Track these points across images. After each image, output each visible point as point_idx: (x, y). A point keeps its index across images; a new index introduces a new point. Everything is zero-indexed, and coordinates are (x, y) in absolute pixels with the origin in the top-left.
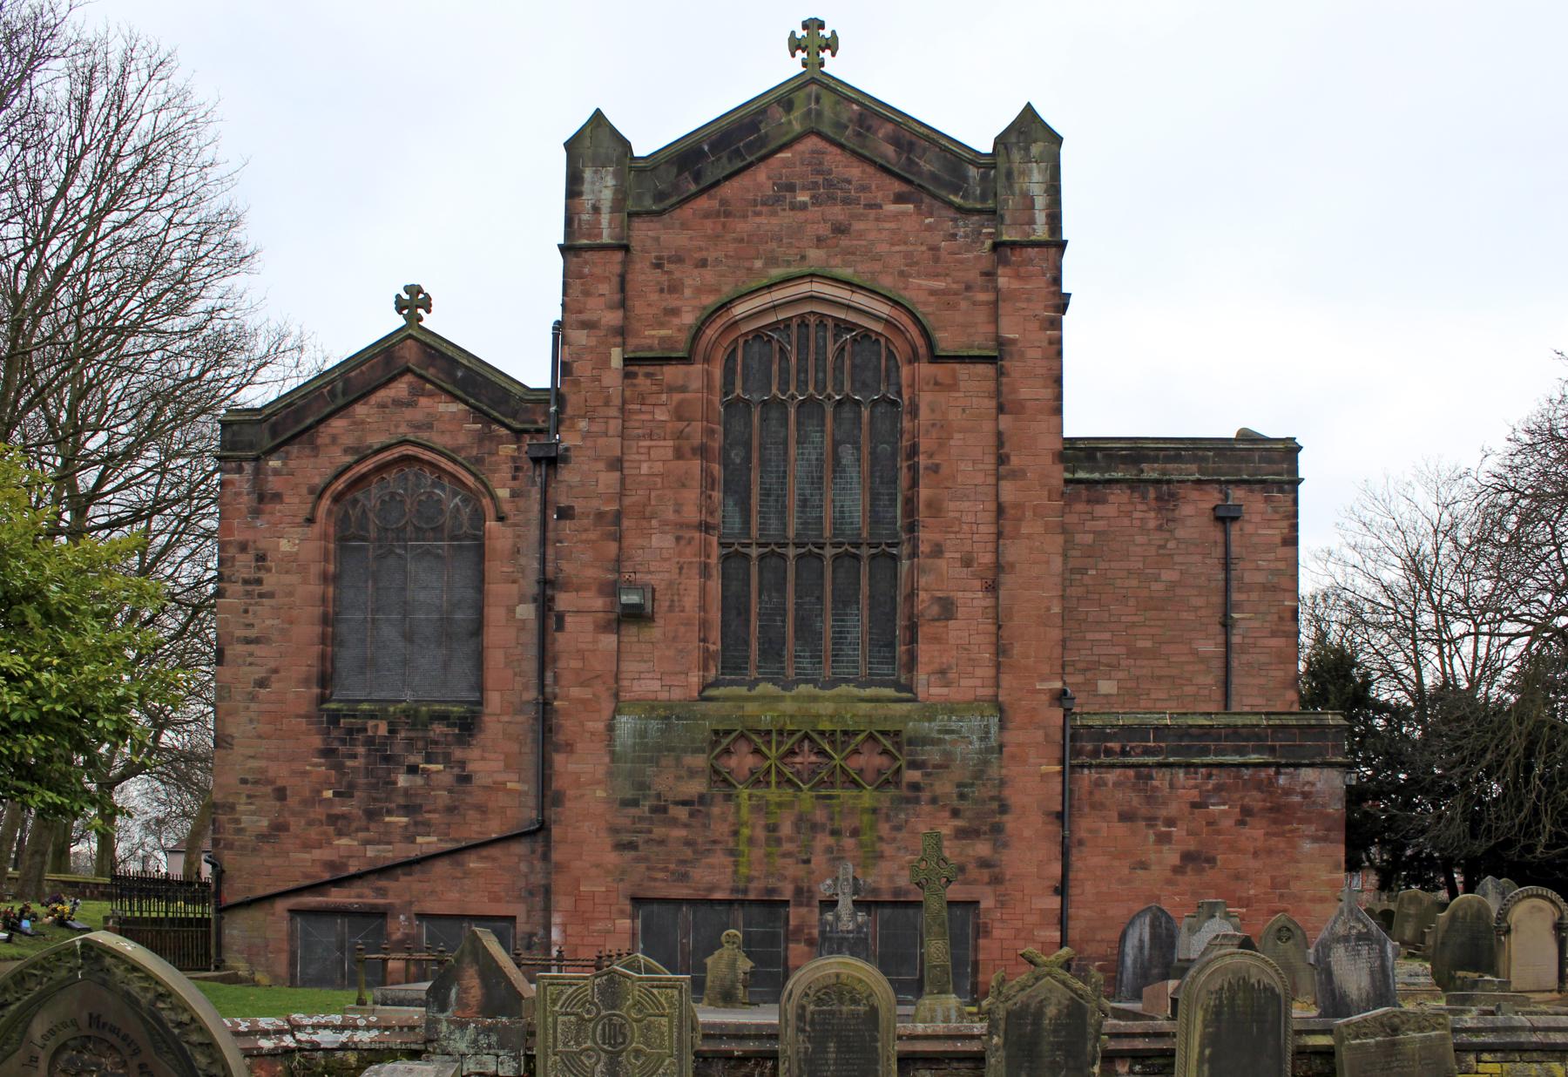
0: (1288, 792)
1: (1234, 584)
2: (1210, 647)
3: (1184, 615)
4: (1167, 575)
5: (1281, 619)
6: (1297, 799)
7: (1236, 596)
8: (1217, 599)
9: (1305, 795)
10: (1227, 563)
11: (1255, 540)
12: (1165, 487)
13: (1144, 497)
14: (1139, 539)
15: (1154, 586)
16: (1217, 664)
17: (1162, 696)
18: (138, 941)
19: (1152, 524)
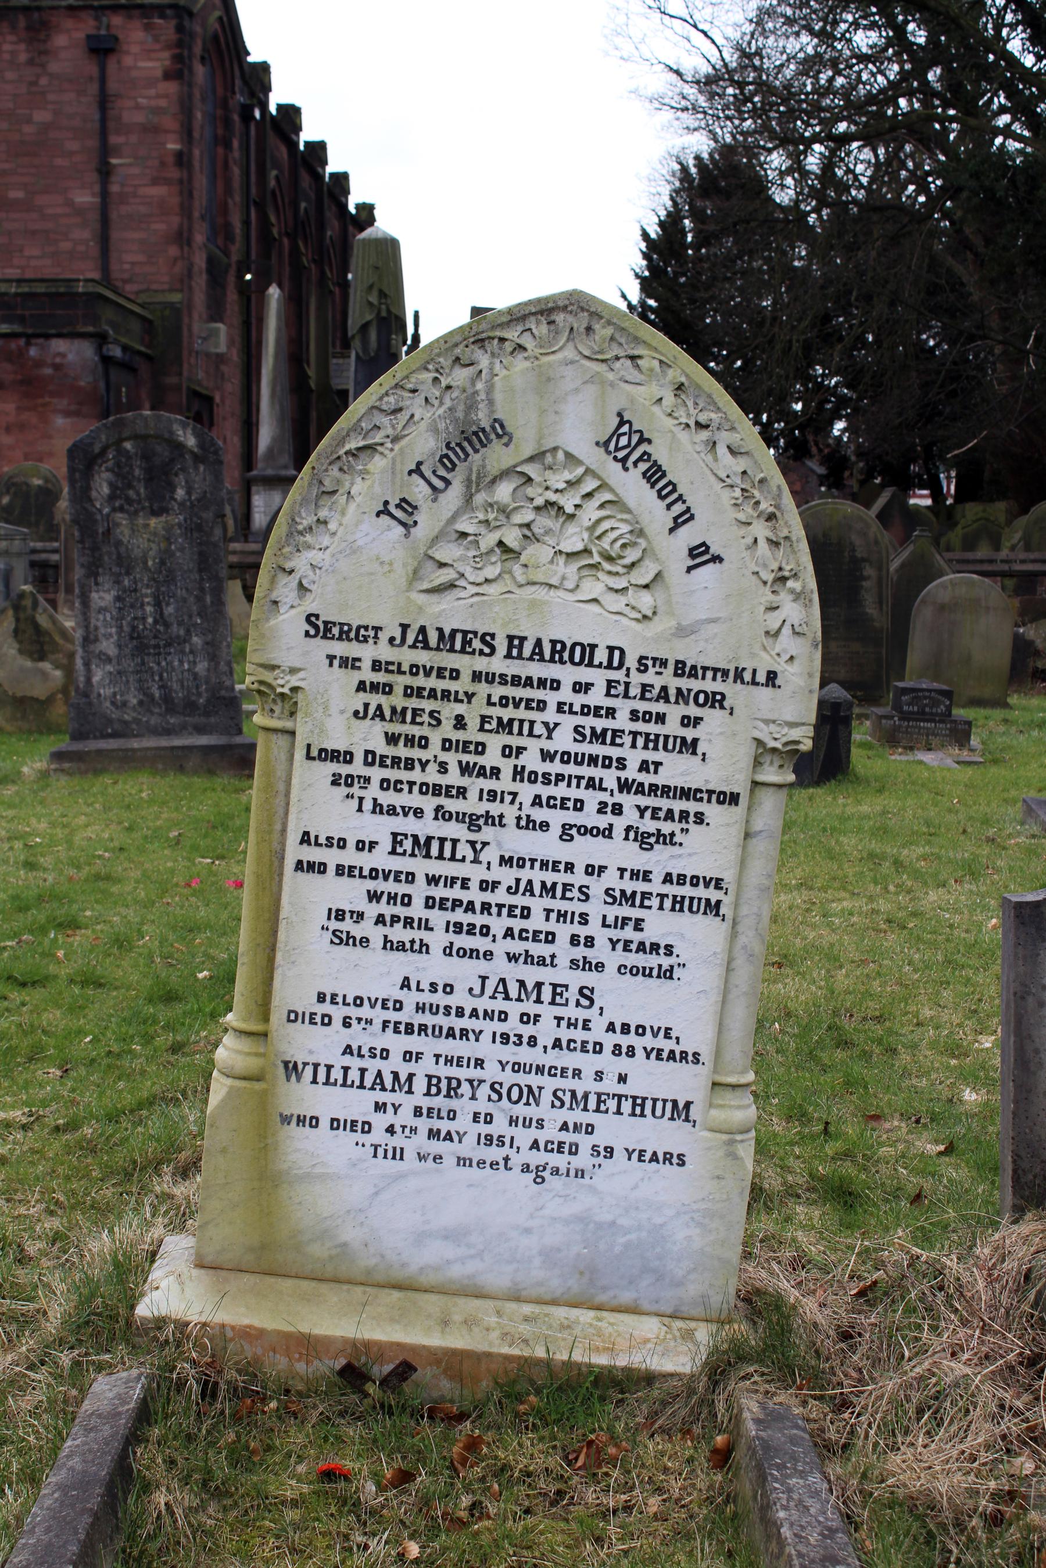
0: (39, 364)
1: (111, 125)
2: (86, 198)
3: (59, 162)
4: (41, 116)
5: (163, 164)
6: (48, 371)
7: (114, 139)
8: (93, 143)
9: (57, 367)
10: (104, 101)
11: (134, 74)
12: (36, 15)
13: (14, 28)
14: (10, 75)
15: (27, 129)
16: (94, 216)
17: (36, 252)
18: (823, 619)
19: (23, 57)
